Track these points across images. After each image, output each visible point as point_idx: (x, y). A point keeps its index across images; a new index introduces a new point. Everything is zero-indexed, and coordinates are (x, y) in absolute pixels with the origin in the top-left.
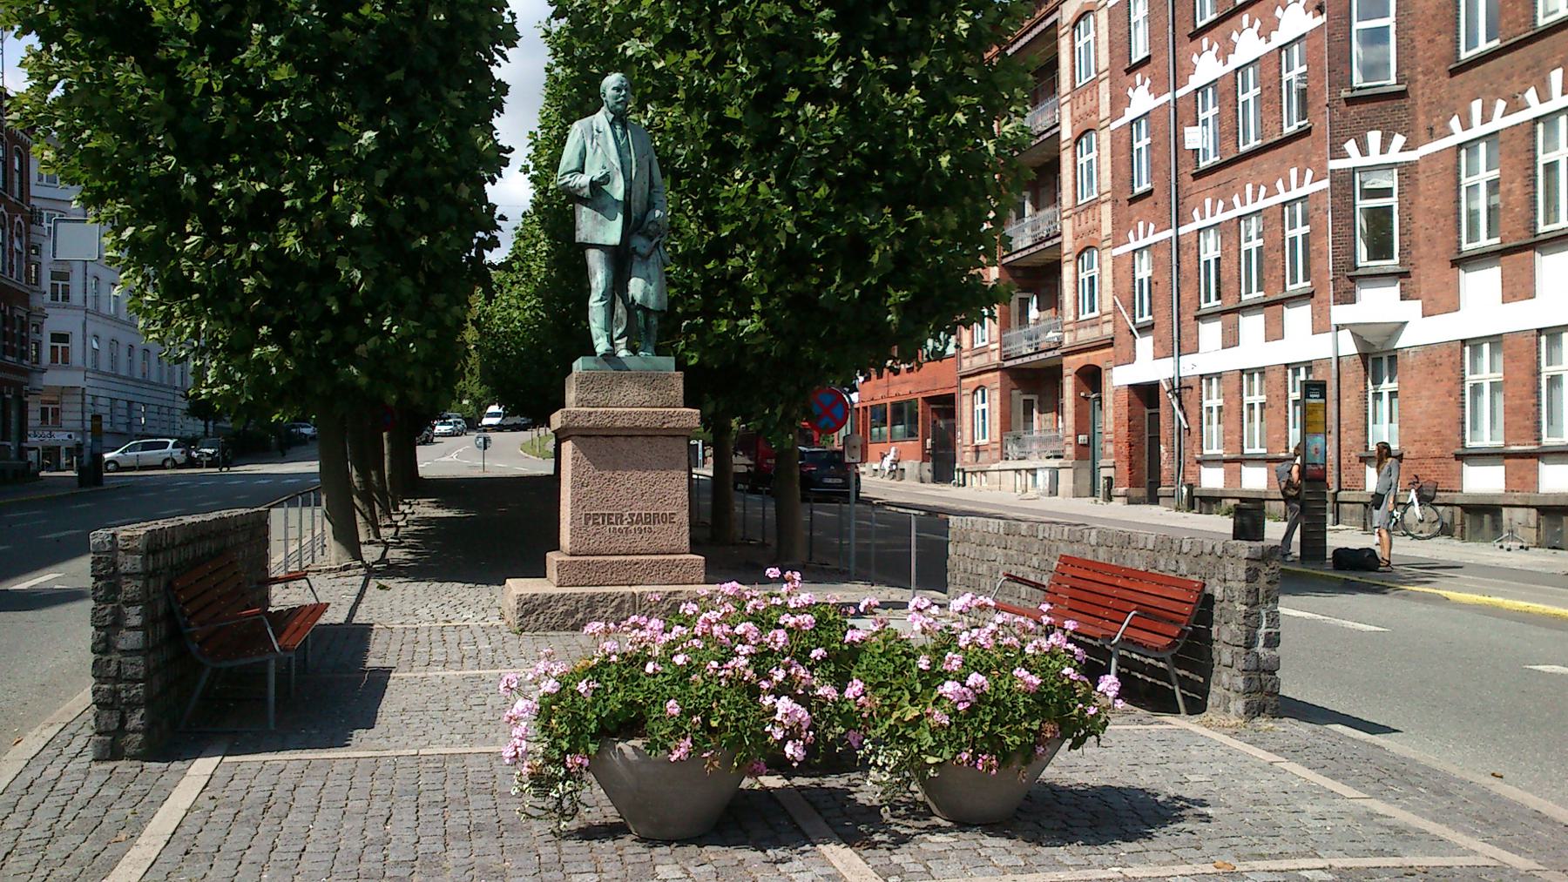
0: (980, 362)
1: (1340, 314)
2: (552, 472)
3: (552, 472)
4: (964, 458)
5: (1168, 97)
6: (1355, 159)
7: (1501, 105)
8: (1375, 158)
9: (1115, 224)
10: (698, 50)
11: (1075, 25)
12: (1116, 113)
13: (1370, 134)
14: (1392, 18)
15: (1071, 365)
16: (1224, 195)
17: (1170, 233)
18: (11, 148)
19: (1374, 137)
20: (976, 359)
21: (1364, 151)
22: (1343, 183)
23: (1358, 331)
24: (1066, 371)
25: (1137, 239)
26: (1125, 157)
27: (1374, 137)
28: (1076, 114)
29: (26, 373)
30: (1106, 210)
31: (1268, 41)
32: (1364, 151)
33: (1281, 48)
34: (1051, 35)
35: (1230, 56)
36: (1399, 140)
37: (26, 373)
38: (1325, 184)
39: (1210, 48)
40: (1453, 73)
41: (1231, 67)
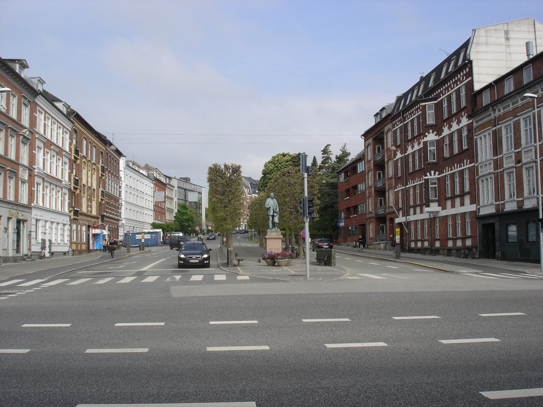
0: (370, 215)
1: (426, 209)
4: (368, 241)
5: (403, 155)
6: (429, 177)
7: (437, 173)
8: (433, 176)
9: (395, 184)
10: (268, 228)
11: (387, 133)
12: (395, 157)
13: (432, 171)
14: (435, 147)
15: (388, 217)
16: (451, 166)
17: (404, 187)
19: (433, 172)
20: (370, 215)
21: (431, 175)
22: (427, 181)
23: (430, 213)
24: (387, 219)
25: (446, 172)
26: (396, 168)
27: (433, 172)
28: (388, 155)
29: (118, 220)
30: (393, 179)
31: (459, 126)
32: (431, 175)
33: (462, 127)
34: (383, 133)
35: (460, 124)
36: (437, 173)
37: (118, 220)
38: (423, 181)
39: (464, 115)
40: (444, 160)
41: (451, 132)
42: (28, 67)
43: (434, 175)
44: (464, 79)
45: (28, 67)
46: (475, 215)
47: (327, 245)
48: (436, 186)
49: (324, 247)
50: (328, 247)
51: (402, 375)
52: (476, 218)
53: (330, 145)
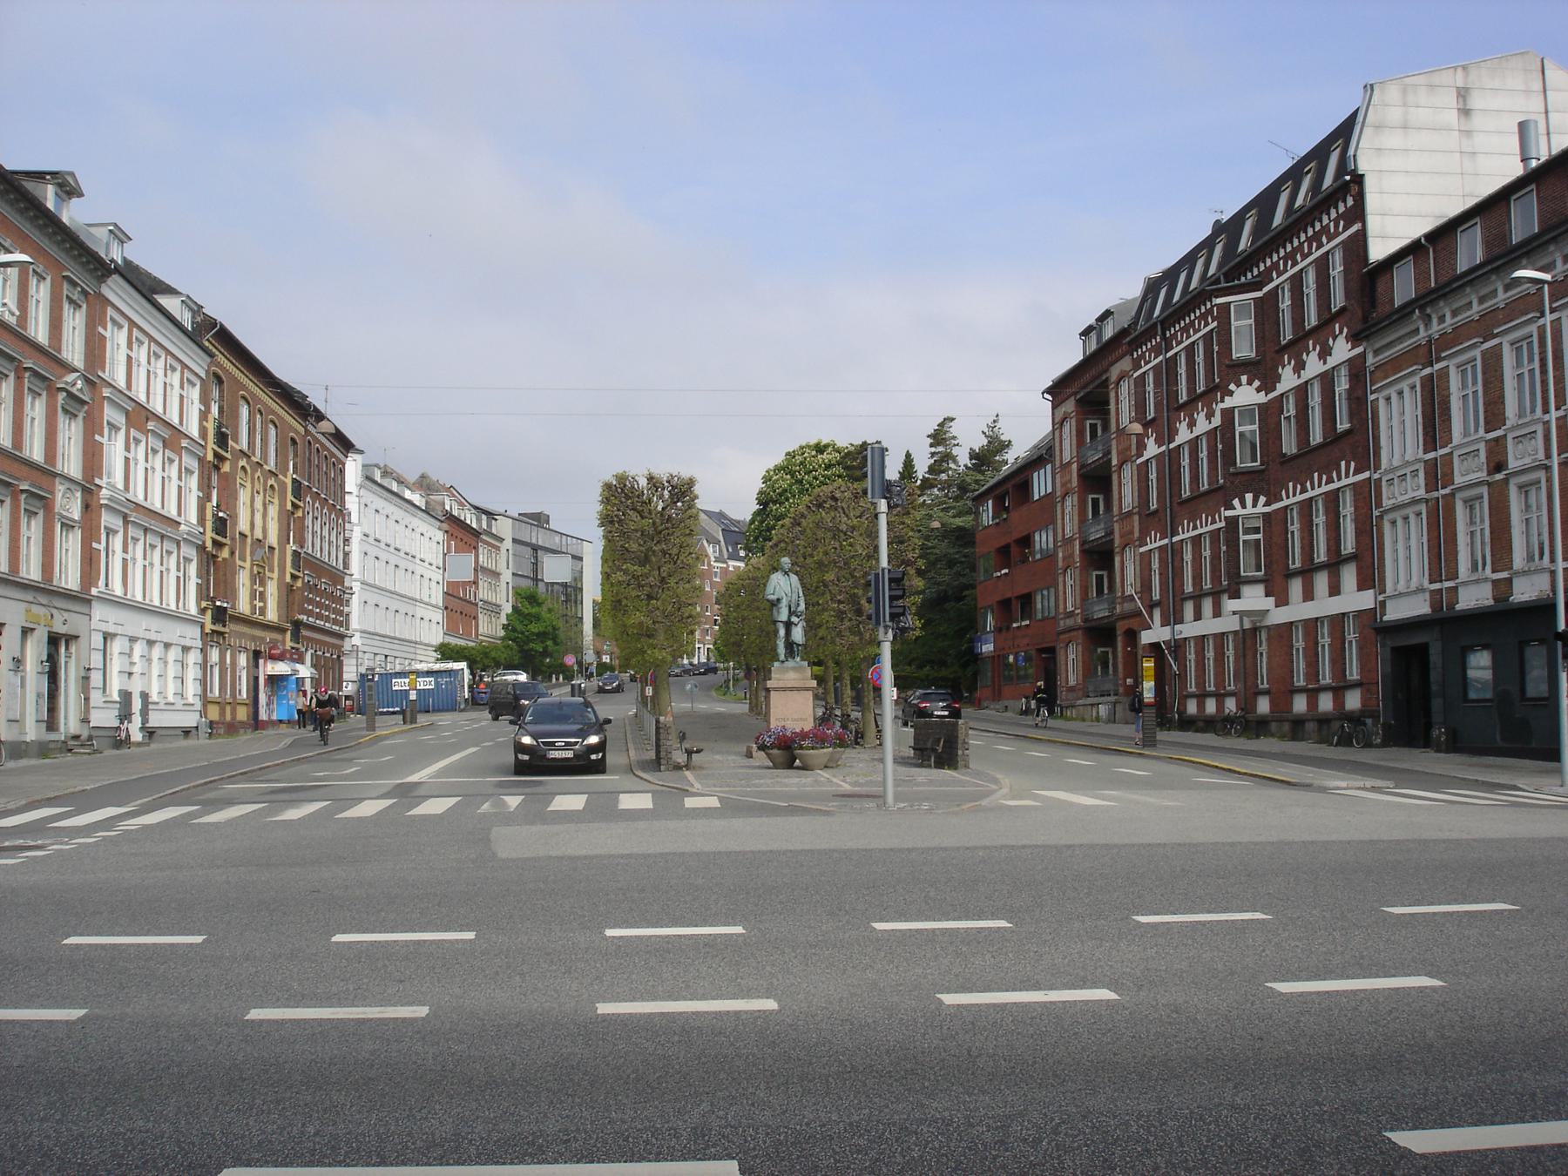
0: (1070, 622)
1: (1230, 605)
2: (811, 692)
3: (811, 692)
4: (1062, 697)
5: (1163, 448)
6: (1239, 511)
7: (1262, 499)
8: (1249, 510)
9: (1141, 531)
11: (1118, 383)
12: (1140, 455)
13: (1247, 495)
14: (1257, 425)
15: (1121, 628)
16: (1302, 480)
17: (1166, 541)
18: (254, 408)
19: (1249, 497)
20: (1068, 620)
21: (1244, 506)
22: (1232, 523)
24: (1118, 632)
25: (1288, 497)
26: (1143, 484)
27: (1249, 497)
28: (1120, 448)
29: (342, 637)
30: (1136, 518)
31: (1325, 363)
32: (1244, 506)
33: (1333, 368)
35: (1328, 358)
36: (1262, 499)
37: (342, 637)
38: (1223, 524)
39: (1341, 332)
40: (1282, 463)
41: (1302, 381)
42: (81, 195)
43: (1254, 505)
44: (1341, 229)
45: (81, 195)
46: (1370, 622)
47: (943, 709)
48: (1260, 536)
49: (936, 713)
50: (946, 713)
51: (1161, 1082)
52: (1375, 629)
53: (953, 419)
